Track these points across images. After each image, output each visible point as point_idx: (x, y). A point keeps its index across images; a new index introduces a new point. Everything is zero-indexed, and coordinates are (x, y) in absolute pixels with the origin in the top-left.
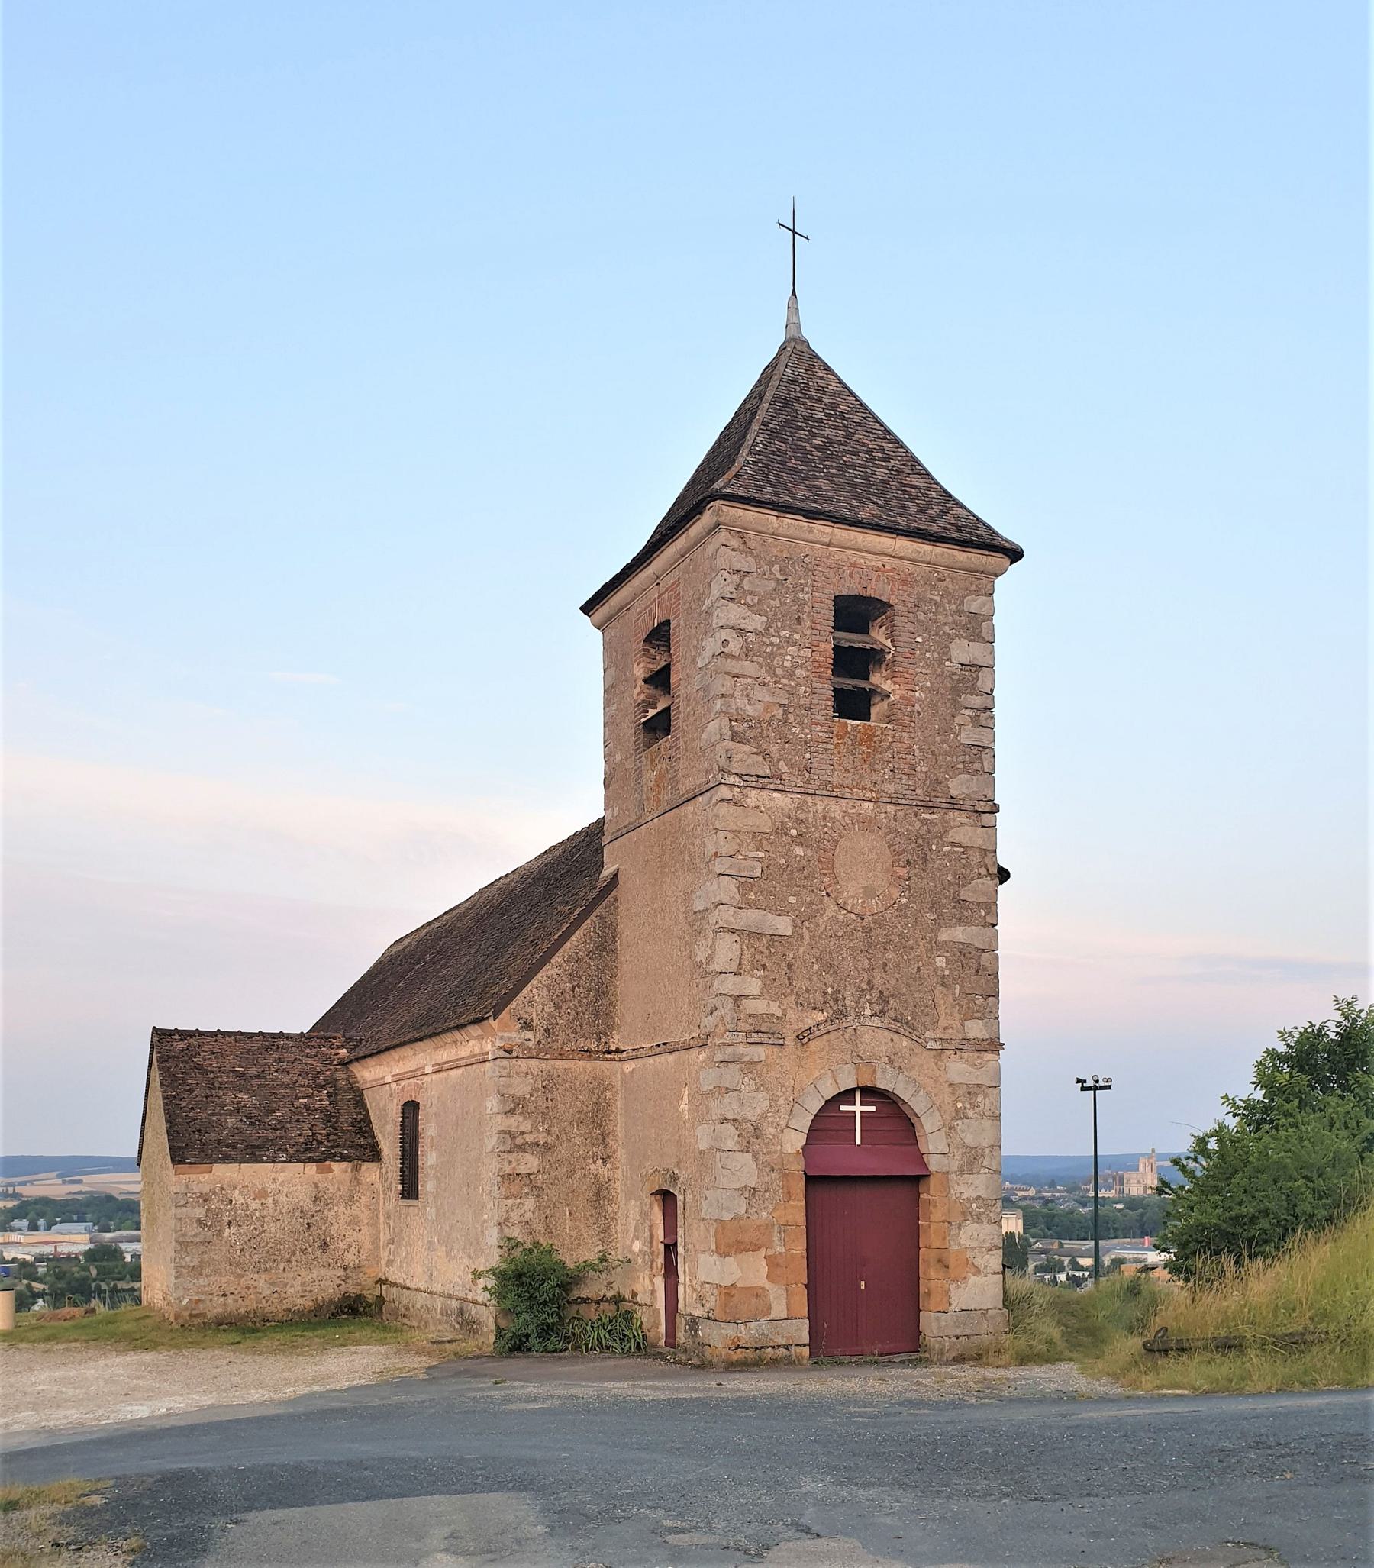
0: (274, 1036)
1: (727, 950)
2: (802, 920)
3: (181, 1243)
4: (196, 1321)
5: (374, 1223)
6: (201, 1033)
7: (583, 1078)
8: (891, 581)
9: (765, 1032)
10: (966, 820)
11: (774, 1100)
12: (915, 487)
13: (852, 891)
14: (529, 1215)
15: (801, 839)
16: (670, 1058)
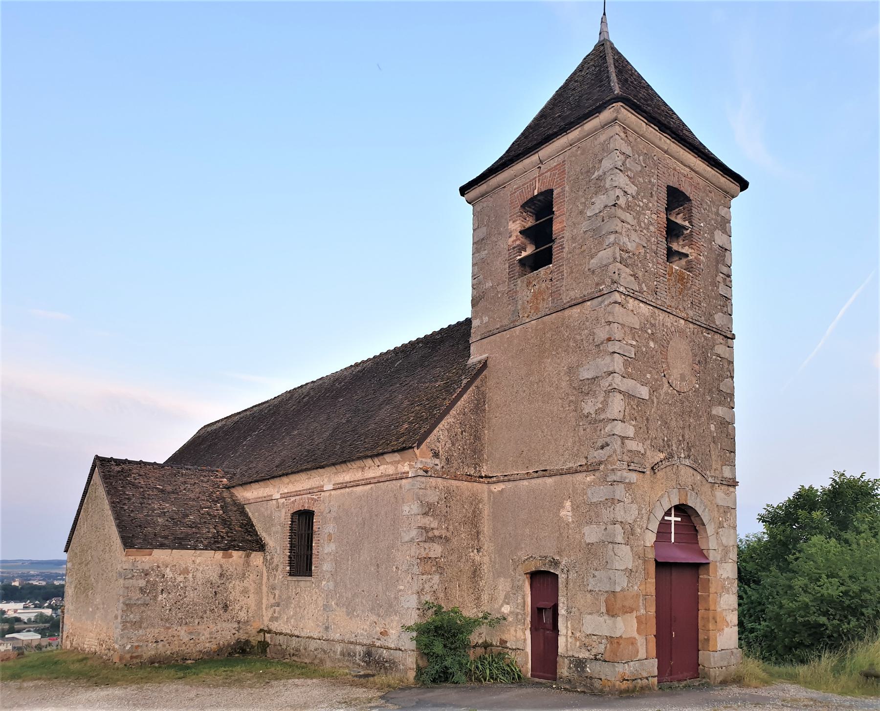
1: (617, 405)
2: (654, 390)
3: (127, 605)
4: (135, 661)
5: (259, 591)
6: (130, 462)
7: (467, 493)
9: (634, 463)
10: (722, 341)
11: (640, 510)
13: (675, 374)
14: (436, 587)
15: (652, 336)
16: (549, 481)
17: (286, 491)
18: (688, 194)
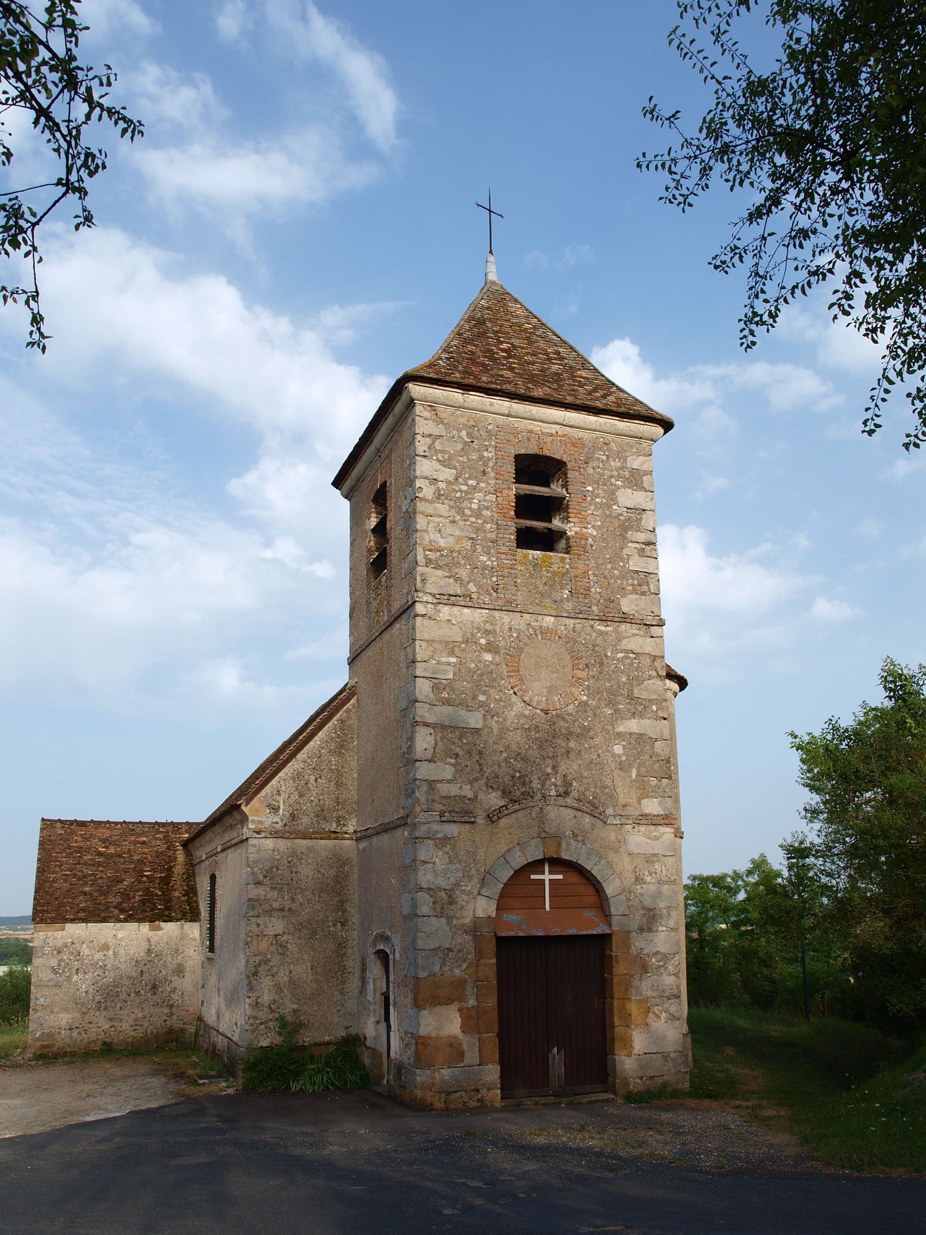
0: (72, 823)
10: (637, 632)
12: (583, 378)
15: (490, 648)
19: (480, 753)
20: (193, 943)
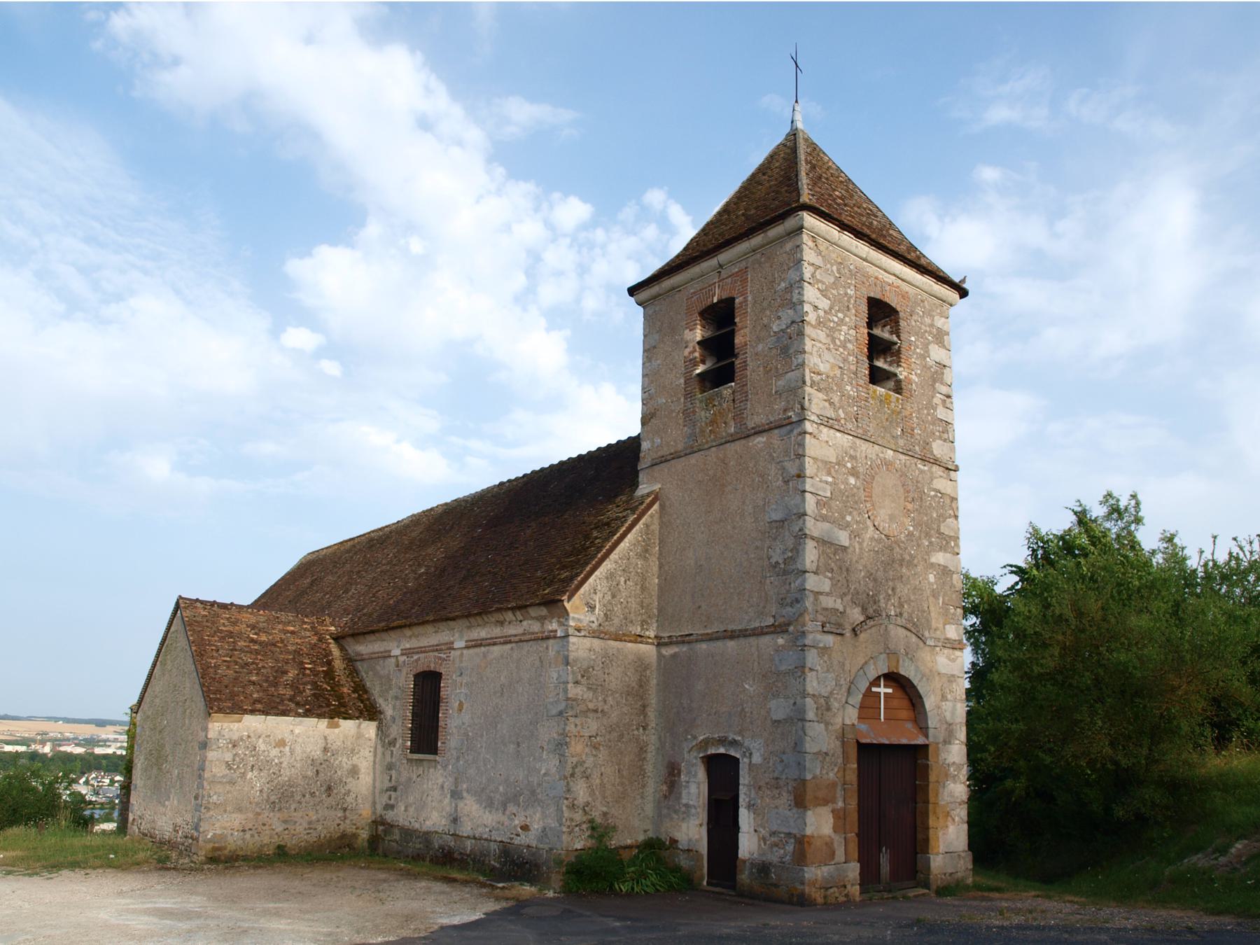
0: (213, 603)
8: (897, 294)
13: (882, 517)
15: (854, 472)
17: (408, 646)
18: (893, 305)
19: (847, 570)
20: (369, 743)
